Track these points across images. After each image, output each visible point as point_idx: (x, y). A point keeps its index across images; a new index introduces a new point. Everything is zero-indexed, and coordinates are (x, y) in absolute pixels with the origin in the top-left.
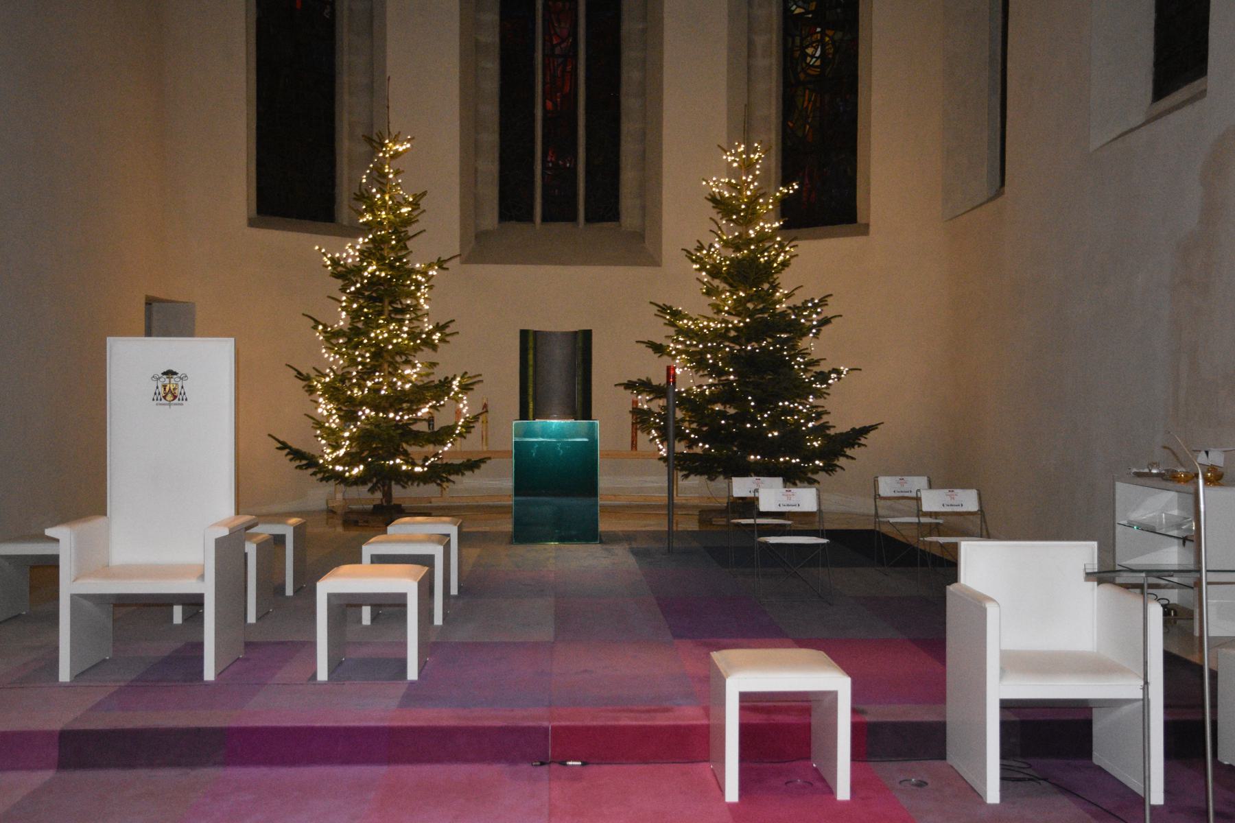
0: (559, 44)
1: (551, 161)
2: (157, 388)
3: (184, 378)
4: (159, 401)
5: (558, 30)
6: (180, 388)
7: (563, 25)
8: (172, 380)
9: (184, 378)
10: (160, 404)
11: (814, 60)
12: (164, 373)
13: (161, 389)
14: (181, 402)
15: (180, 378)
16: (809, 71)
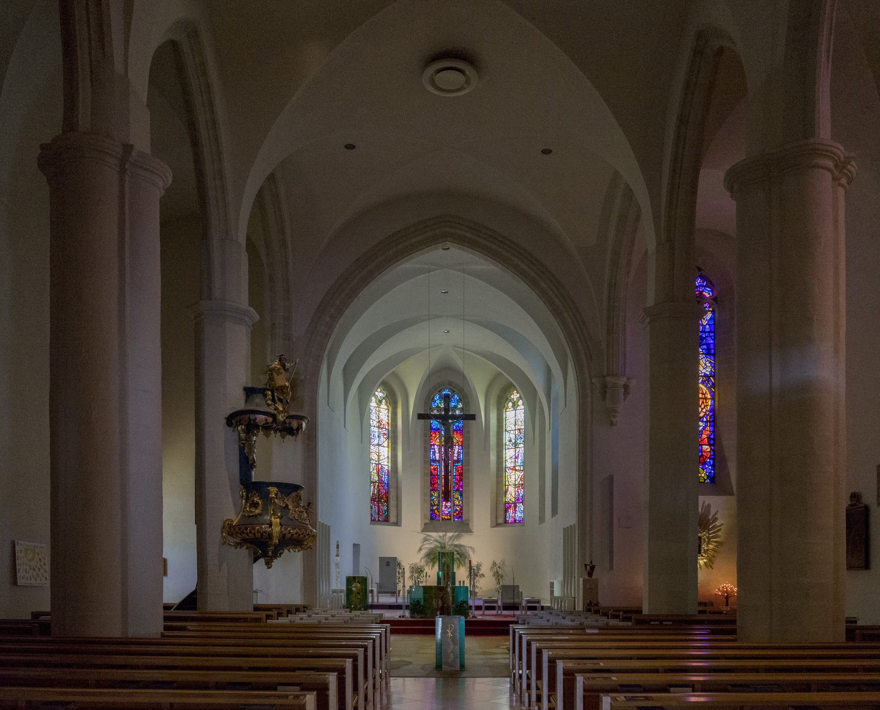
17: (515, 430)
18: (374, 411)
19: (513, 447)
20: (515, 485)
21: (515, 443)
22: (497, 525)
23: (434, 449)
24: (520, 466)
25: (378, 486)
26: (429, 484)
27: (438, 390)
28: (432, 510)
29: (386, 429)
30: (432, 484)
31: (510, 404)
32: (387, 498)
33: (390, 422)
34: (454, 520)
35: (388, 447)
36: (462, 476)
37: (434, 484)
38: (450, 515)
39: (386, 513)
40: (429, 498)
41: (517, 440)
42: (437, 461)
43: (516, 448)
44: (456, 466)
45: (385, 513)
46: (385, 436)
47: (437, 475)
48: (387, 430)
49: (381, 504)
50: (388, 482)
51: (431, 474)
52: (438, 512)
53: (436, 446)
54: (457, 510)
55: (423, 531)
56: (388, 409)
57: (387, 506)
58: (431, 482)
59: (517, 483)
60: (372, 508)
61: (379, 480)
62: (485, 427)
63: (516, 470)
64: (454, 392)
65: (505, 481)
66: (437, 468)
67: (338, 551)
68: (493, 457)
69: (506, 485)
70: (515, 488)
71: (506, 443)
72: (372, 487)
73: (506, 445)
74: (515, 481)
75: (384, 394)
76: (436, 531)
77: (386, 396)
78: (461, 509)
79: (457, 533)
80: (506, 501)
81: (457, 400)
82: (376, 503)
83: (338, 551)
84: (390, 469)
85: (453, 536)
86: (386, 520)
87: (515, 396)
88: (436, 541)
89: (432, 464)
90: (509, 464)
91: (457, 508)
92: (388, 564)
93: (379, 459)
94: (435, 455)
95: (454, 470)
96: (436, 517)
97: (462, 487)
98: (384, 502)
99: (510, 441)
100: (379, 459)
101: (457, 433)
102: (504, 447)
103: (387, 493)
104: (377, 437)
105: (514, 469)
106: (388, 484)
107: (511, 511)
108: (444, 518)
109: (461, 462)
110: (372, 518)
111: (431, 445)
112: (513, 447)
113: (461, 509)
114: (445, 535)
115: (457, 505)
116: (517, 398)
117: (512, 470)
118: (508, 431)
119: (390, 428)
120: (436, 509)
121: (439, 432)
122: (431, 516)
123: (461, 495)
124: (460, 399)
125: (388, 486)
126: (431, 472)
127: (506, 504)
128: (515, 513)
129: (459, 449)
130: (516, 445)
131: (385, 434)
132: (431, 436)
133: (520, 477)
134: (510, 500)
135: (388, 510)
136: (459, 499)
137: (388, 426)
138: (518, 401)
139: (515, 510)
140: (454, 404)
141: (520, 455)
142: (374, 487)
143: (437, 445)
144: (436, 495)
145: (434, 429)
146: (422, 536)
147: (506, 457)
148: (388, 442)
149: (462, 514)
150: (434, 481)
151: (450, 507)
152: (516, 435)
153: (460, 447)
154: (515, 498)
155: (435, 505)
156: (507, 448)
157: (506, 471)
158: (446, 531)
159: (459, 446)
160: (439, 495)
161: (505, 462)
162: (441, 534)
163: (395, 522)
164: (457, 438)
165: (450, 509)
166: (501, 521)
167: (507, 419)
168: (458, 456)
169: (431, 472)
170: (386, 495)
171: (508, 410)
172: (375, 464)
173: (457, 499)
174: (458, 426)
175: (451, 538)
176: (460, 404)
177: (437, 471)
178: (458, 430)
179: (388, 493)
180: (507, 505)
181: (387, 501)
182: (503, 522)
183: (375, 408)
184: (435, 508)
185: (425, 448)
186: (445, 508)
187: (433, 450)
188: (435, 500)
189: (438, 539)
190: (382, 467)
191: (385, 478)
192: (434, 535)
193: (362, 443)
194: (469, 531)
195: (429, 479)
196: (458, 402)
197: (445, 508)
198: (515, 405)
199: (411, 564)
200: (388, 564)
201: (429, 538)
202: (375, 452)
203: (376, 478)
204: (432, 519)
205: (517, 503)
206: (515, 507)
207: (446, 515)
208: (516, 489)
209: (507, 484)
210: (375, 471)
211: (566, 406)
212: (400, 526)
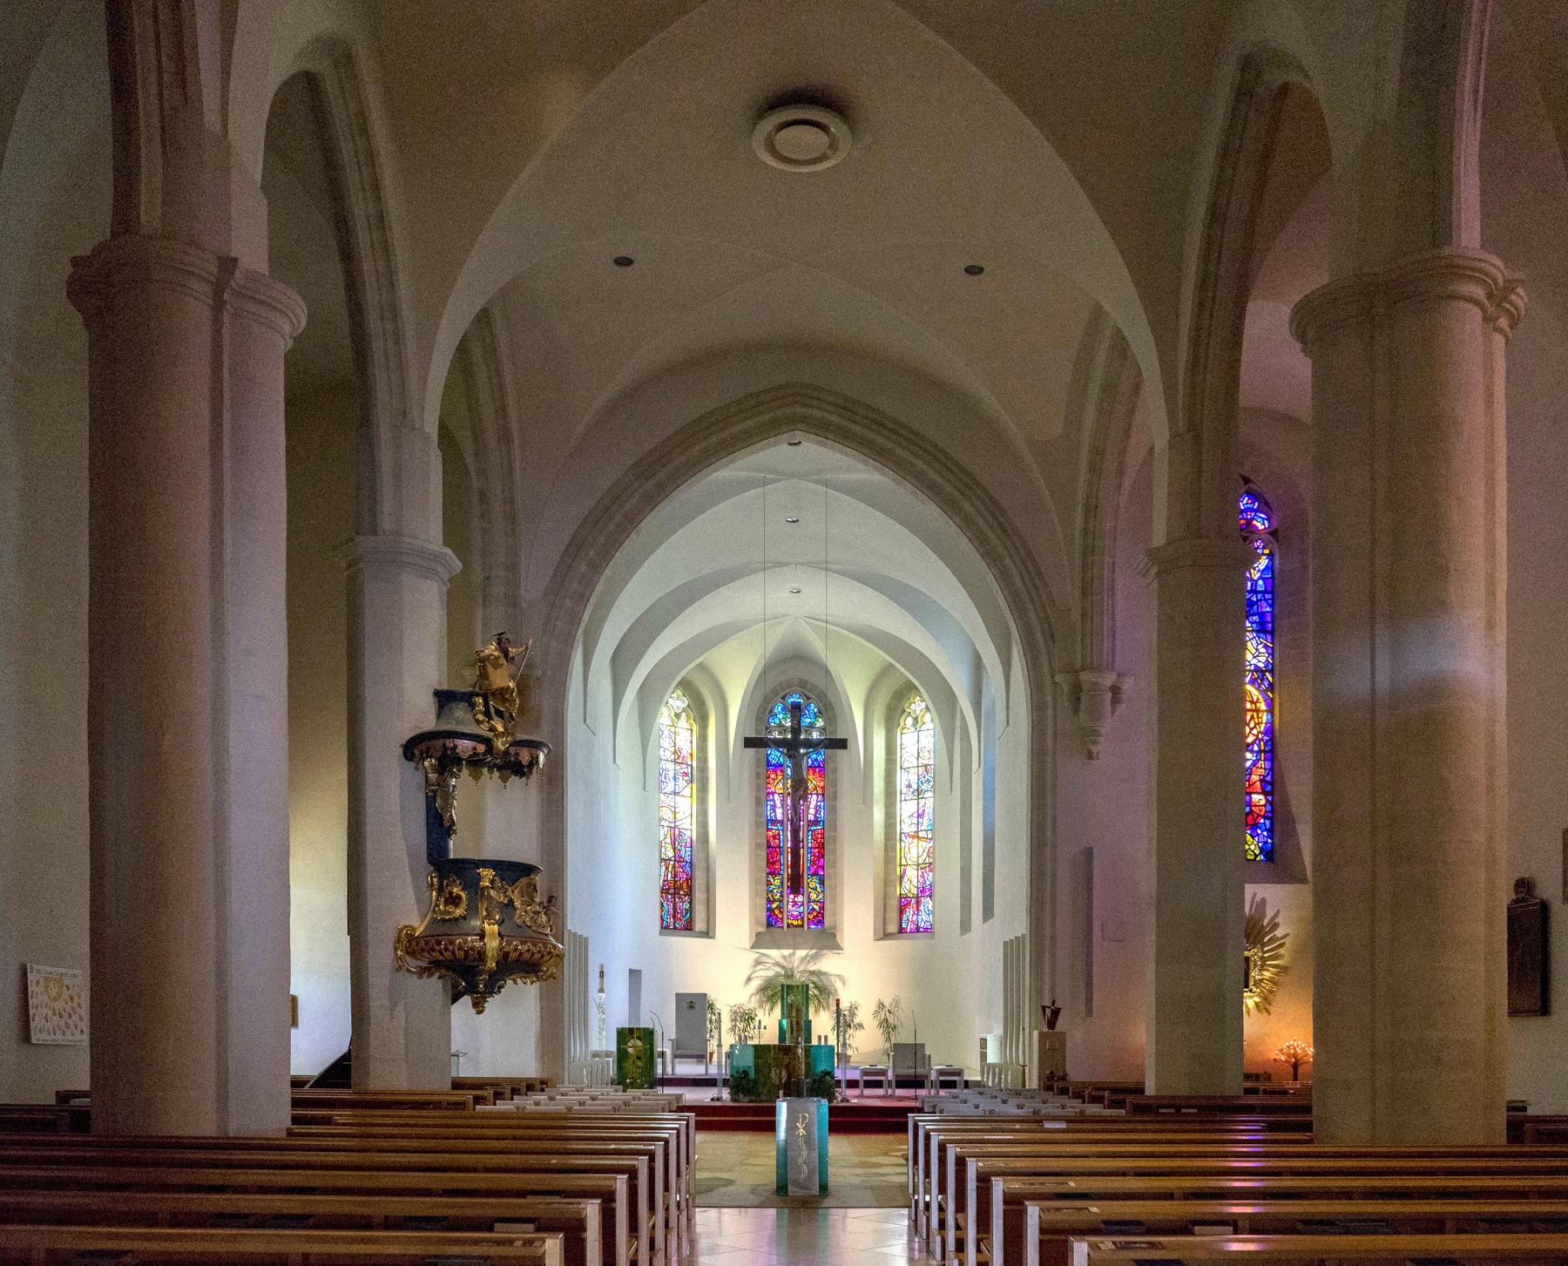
17: (918, 767)
22: (886, 936)
23: (773, 800)
25: (674, 866)
26: (764, 863)
27: (782, 694)
28: (770, 910)
29: (688, 765)
31: (909, 721)
32: (690, 887)
34: (809, 928)
36: (823, 848)
37: (774, 863)
39: (688, 916)
41: (920, 784)
42: (779, 822)
43: (919, 798)
44: (813, 831)
46: (686, 778)
47: (779, 847)
48: (689, 767)
49: (679, 898)
52: (781, 912)
54: (813, 909)
57: (691, 903)
58: (768, 860)
59: (921, 861)
61: (675, 856)
62: (865, 762)
63: (918, 837)
66: (779, 834)
67: (602, 983)
68: (878, 815)
76: (778, 947)
77: (688, 706)
78: (822, 908)
79: (814, 951)
80: (901, 894)
82: (669, 896)
85: (806, 956)
86: (688, 927)
88: (777, 964)
90: (908, 828)
91: (815, 907)
92: (691, 1006)
94: (775, 811)
97: (823, 868)
98: (685, 896)
99: (909, 786)
101: (815, 772)
103: (690, 879)
105: (916, 836)
108: (792, 924)
111: (769, 793)
114: (794, 954)
115: (814, 901)
117: (913, 837)
123: (822, 883)
126: (768, 842)
129: (817, 801)
132: (768, 777)
133: (927, 851)
135: (691, 910)
136: (819, 890)
140: (809, 720)
142: (667, 868)
145: (774, 765)
146: (753, 955)
150: (773, 858)
151: (802, 905)
153: (820, 797)
154: (918, 888)
155: (775, 900)
158: (795, 947)
159: (817, 794)
162: (786, 952)
163: (704, 930)
165: (802, 908)
166: (893, 928)
173: (815, 889)
175: (803, 959)
176: (820, 720)
177: (779, 839)
179: (691, 879)
180: (903, 900)
181: (690, 893)
182: (896, 931)
184: (774, 906)
186: (793, 906)
187: (772, 803)
188: (775, 891)
189: (781, 961)
193: (644, 789)
194: (836, 947)
195: (763, 853)
197: (793, 906)
200: (691, 1006)
201: (764, 959)
204: (769, 925)
206: (918, 904)
207: (796, 918)
212: (713, 937)
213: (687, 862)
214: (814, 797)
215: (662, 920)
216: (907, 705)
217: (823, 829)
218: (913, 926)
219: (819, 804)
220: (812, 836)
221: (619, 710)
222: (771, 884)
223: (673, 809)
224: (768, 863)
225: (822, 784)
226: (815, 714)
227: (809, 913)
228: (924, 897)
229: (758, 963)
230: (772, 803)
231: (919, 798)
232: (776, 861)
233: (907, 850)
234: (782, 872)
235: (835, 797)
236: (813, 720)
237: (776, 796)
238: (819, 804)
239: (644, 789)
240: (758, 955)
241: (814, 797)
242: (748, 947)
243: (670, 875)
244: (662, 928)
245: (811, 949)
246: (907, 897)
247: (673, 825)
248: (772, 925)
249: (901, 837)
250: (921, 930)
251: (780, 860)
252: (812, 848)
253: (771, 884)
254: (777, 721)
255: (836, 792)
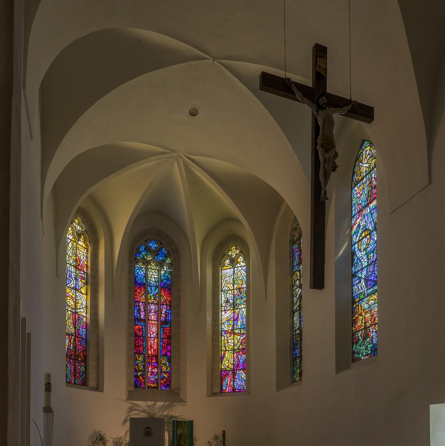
0: (153, 334)
1: (150, 370)
2: (145, 432)
3: (152, 429)
4: (145, 436)
5: (152, 330)
6: (151, 432)
7: (154, 328)
8: (149, 430)
9: (152, 429)
10: (146, 437)
11: (231, 344)
12: (146, 428)
13: (145, 432)
14: (151, 436)
15: (151, 429)
16: (230, 347)
17: (234, 289)
18: (70, 245)
19: (231, 309)
20: (234, 350)
21: (234, 303)
22: (213, 394)
23: (139, 306)
24: (240, 329)
25: (75, 340)
26: (133, 345)
27: (145, 239)
28: (136, 377)
29: (84, 272)
30: (137, 346)
31: (227, 261)
32: (85, 356)
33: (89, 264)
34: (161, 389)
35: (86, 294)
36: (170, 340)
37: (139, 346)
38: (157, 383)
39: (84, 376)
40: (133, 361)
41: (235, 300)
42: (142, 320)
43: (234, 309)
44: (164, 328)
45: (82, 375)
46: (84, 281)
47: (142, 336)
48: (85, 274)
49: (78, 363)
50: (86, 337)
51: (136, 335)
52: (143, 378)
53: (141, 304)
54: (164, 377)
55: (128, 399)
56: (87, 250)
57: (86, 367)
58: (135, 344)
59: (236, 348)
60: (67, 367)
61: (75, 333)
62: (201, 282)
63: (234, 334)
64: (162, 244)
65: (221, 347)
66: (142, 328)
67: (48, 399)
68: (209, 318)
69: (222, 351)
70: (234, 353)
71: (222, 305)
72: (67, 341)
73: (222, 306)
74: (234, 346)
75: (82, 228)
76: (144, 400)
77: (86, 231)
78: (170, 376)
79: (168, 403)
80: (222, 369)
81: (165, 254)
82: (71, 361)
83: (48, 399)
84: (88, 322)
85: (163, 405)
86: (84, 384)
87: (234, 252)
88: (144, 411)
89: (136, 323)
90: (226, 327)
91: (165, 376)
92: (148, 433)
93: (75, 306)
94: (140, 313)
95: (162, 332)
96: (141, 384)
97: (170, 351)
98: (82, 362)
99: (227, 302)
100: (75, 306)
101: (165, 290)
102: (220, 308)
103: (85, 350)
104: (73, 279)
105: (232, 332)
106: (86, 340)
107: (228, 380)
108: (150, 386)
109: (169, 324)
110: (67, 380)
111: (136, 302)
112: (231, 309)
113: (170, 376)
114: (155, 404)
115: (165, 372)
116: (236, 254)
117: (230, 333)
118: (224, 291)
119: (89, 272)
120: (140, 375)
121: (144, 288)
122: (135, 383)
123: (170, 362)
124: (168, 253)
125: (86, 343)
126: (135, 332)
127: (222, 371)
128: (234, 381)
129: (167, 310)
130: (234, 306)
131: (84, 279)
132: (136, 291)
133: (240, 341)
134: (228, 367)
135: (86, 372)
136: (167, 365)
137: (87, 270)
138: (238, 258)
139: (234, 378)
140: (161, 258)
141: (240, 317)
142: (70, 341)
143: (142, 302)
144: (141, 359)
145: (140, 284)
146: (127, 405)
147: (221, 320)
148: (87, 289)
149: (170, 382)
150: (138, 343)
151: (157, 374)
152: (234, 295)
153: (168, 307)
154: (234, 365)
155: (139, 371)
156: (223, 310)
157: (222, 335)
158: (156, 400)
159: (167, 305)
160: (144, 359)
161: (221, 326)
162: (150, 403)
163: (96, 387)
164: (165, 297)
165: (157, 376)
166: (217, 390)
167: (223, 278)
168: (166, 316)
169: (135, 332)
170: (83, 354)
171: (224, 268)
172: (70, 311)
173: (165, 364)
174: (166, 283)
175: (161, 408)
176: (169, 259)
177: (142, 332)
178: (166, 288)
179: (86, 351)
180: (223, 372)
181: (85, 360)
182: (219, 391)
183: (72, 242)
184: (139, 374)
185: (130, 304)
186: (151, 375)
187: (138, 308)
188: (140, 364)
189: (146, 408)
190: (79, 317)
191: (83, 332)
192: (142, 403)
193: (57, 276)
194: (182, 401)
195: (133, 339)
196: (166, 257)
197: (151, 375)
198: (233, 262)
199: (114, 438)
200: (148, 433)
201: (136, 407)
202: (71, 297)
203: (73, 331)
204: (136, 386)
205: (236, 370)
206: (234, 374)
207: (153, 382)
208: (235, 355)
209: (223, 348)
210: (71, 321)
211: (430, 182)
212: (102, 391)
213: (83, 339)
214: (165, 306)
215: (67, 377)
216: (226, 251)
217: (170, 327)
218: (231, 389)
219: (168, 311)
220: (163, 331)
221: (45, 182)
222: (137, 360)
223: (74, 300)
224: (135, 346)
225: (169, 298)
226: (165, 254)
227: (161, 380)
228: (238, 370)
229: (131, 410)
230: (138, 308)
231: (234, 309)
232: (141, 345)
233: (226, 342)
234: (144, 353)
235: (179, 306)
236: (164, 259)
237: (141, 304)
238: (168, 311)
239: (57, 276)
240: (131, 404)
241: (165, 306)
242: (125, 398)
243: (72, 345)
244: (66, 382)
245: (166, 402)
246: (226, 370)
247: (74, 311)
248: (138, 387)
249: (221, 334)
250: (237, 390)
251: (143, 345)
252: (163, 339)
253: (137, 360)
254: (141, 256)
255: (179, 304)
